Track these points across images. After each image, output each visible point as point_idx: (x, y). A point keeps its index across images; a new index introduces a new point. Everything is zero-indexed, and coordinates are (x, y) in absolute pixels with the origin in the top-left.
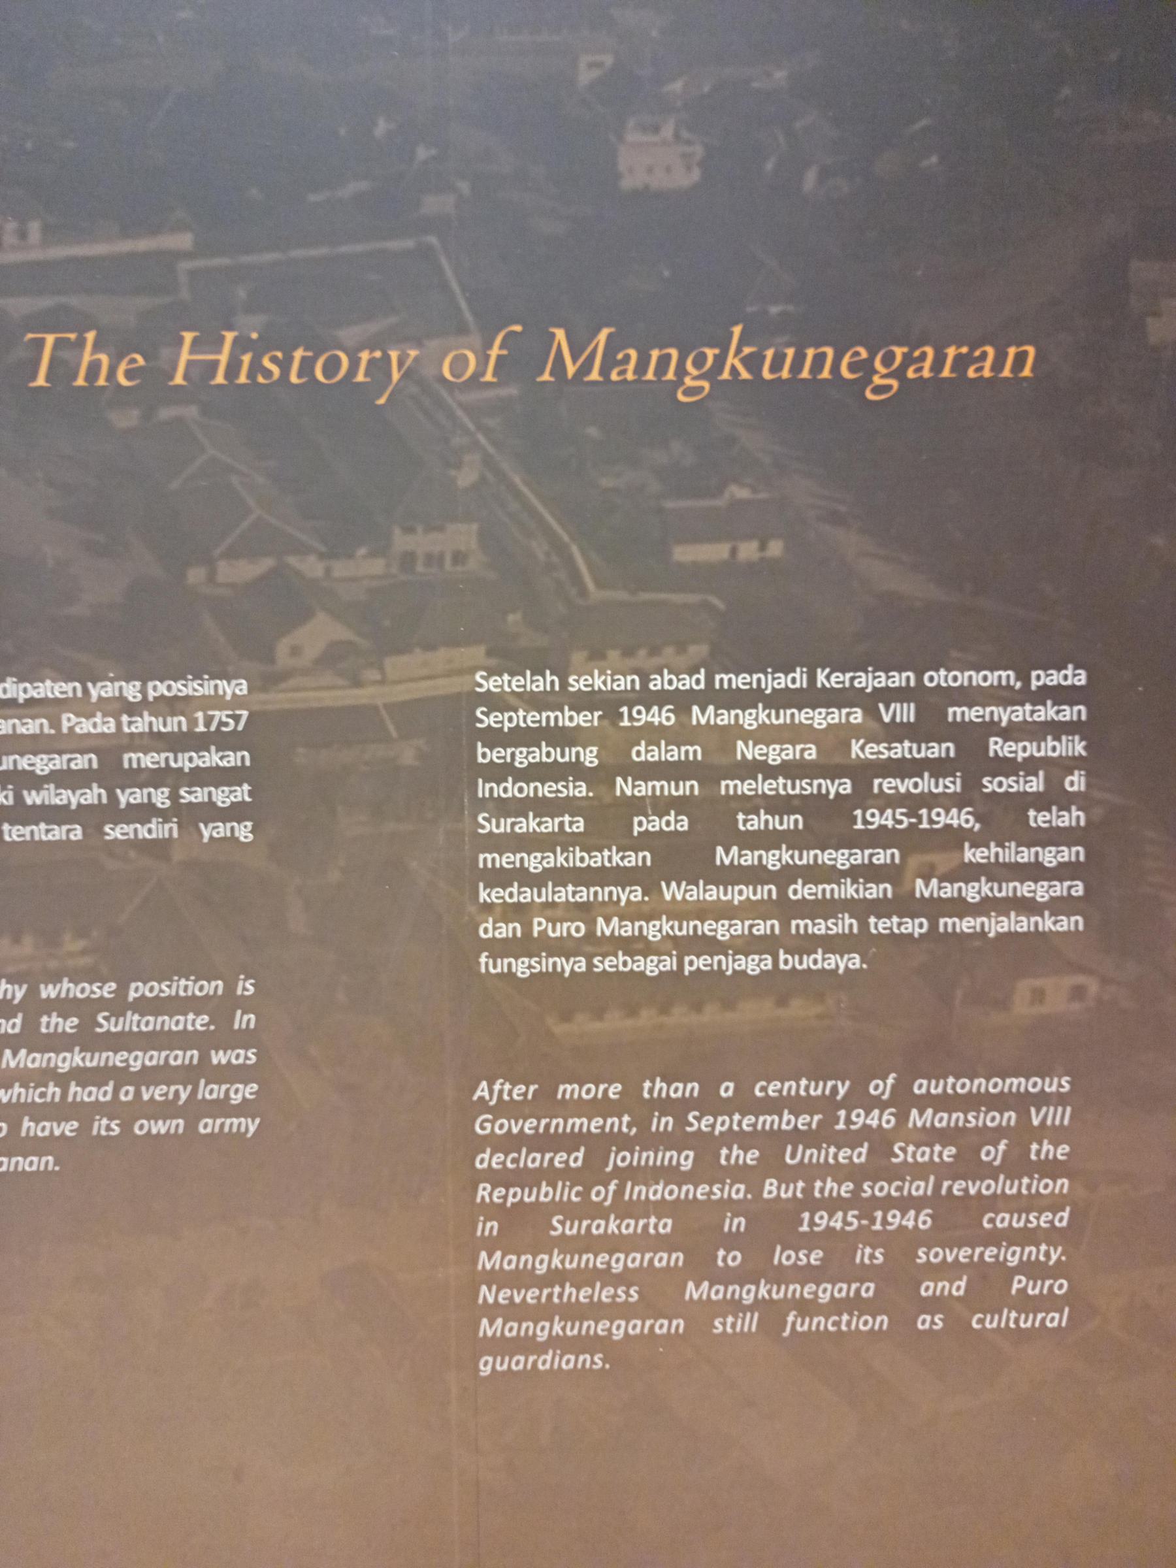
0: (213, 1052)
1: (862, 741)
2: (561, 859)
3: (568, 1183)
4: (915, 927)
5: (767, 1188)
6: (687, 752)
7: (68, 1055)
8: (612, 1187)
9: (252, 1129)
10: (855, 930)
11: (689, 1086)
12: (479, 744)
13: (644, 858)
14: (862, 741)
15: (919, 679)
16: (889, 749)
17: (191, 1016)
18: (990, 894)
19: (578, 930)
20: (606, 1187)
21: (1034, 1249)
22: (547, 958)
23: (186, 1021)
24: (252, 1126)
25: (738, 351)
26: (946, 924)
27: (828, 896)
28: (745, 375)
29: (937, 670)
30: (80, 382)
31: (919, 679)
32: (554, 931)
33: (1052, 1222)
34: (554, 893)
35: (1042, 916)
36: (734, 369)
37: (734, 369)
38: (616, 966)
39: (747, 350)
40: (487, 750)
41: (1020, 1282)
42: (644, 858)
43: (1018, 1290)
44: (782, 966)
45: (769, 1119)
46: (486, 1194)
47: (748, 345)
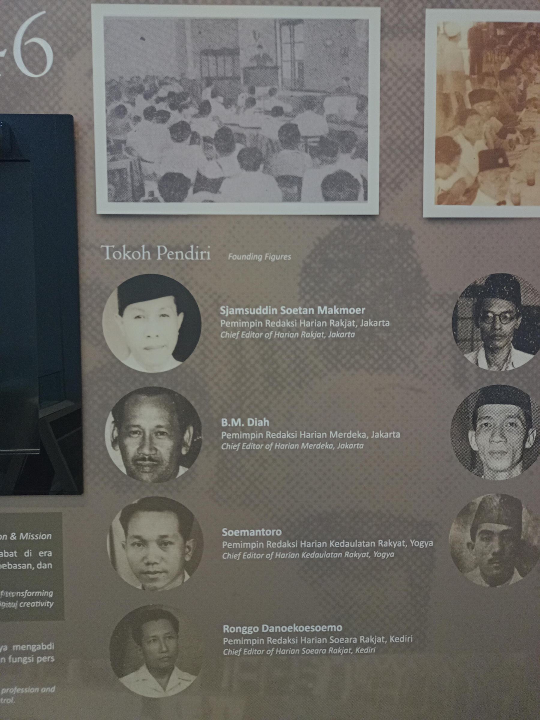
1: (333, 541)
3: (270, 307)
5: (223, 422)
8: (272, 554)
9: (51, 605)
10: (268, 425)
13: (324, 324)
14: (333, 541)
16: (22, 566)
18: (297, 631)
19: (279, 532)
22: (243, 543)
23: (261, 532)
24: (226, 628)
25: (126, 252)
26: (15, 648)
27: (247, 643)
28: (129, 258)
29: (261, 529)
30: (226, 628)
32: (29, 566)
34: (358, 544)
36: (126, 257)
37: (126, 257)
38: (7, 567)
39: (128, 252)
41: (225, 544)
43: (224, 437)
44: (263, 631)
46: (270, 545)
47: (129, 250)
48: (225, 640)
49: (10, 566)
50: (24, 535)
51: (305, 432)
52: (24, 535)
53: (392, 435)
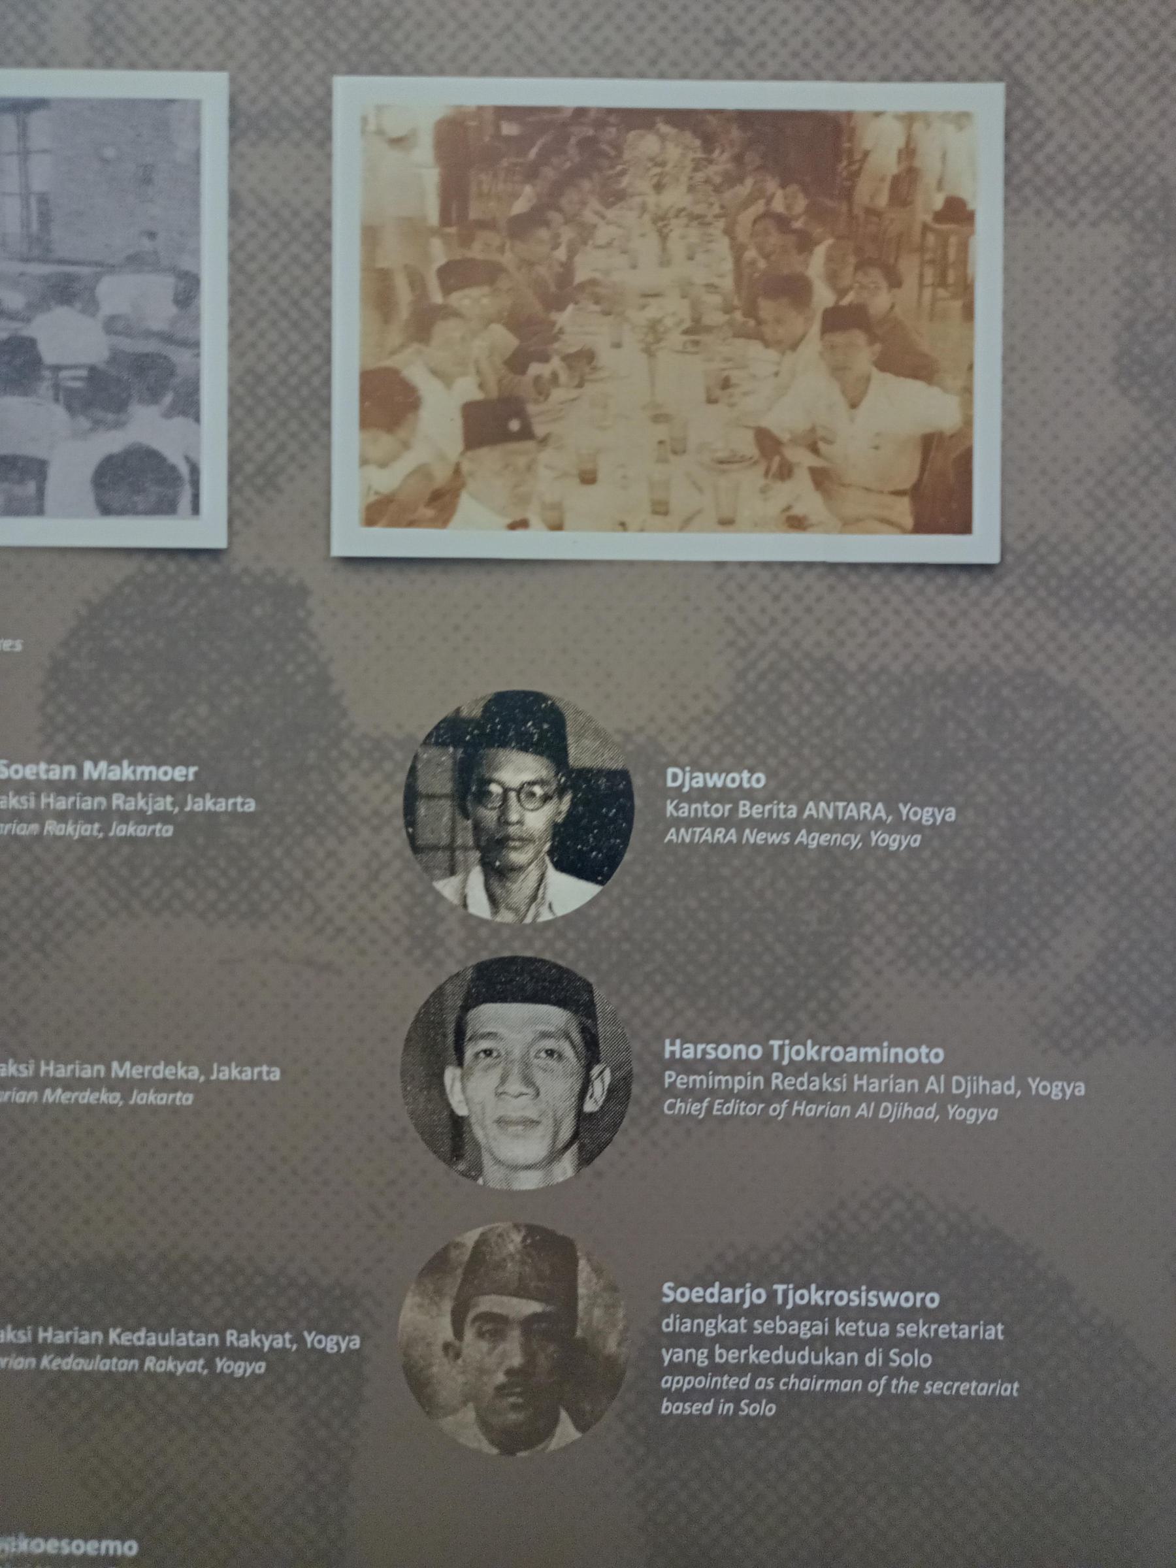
0: (218, 1360)
2: (923, 1331)
4: (120, 1070)
6: (866, 1054)
7: (164, 1362)
8: (883, 1382)
11: (855, 1383)
12: (717, 1346)
15: (862, 1360)
17: (726, 1378)
20: (879, 1381)
21: (719, 1379)
31: (862, 1360)
33: (59, 1366)
35: (805, 1046)
38: (774, 1328)
40: (724, 1351)
42: (913, 1085)
45: (833, 1383)
48: (669, 1077)
49: (782, 1327)
50: (121, 1066)
51: (865, 1077)
52: (121, 1066)
53: (260, 1074)
